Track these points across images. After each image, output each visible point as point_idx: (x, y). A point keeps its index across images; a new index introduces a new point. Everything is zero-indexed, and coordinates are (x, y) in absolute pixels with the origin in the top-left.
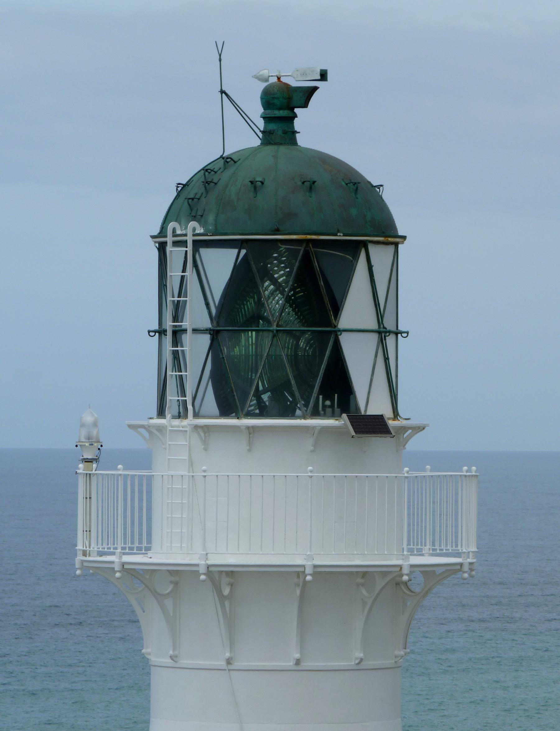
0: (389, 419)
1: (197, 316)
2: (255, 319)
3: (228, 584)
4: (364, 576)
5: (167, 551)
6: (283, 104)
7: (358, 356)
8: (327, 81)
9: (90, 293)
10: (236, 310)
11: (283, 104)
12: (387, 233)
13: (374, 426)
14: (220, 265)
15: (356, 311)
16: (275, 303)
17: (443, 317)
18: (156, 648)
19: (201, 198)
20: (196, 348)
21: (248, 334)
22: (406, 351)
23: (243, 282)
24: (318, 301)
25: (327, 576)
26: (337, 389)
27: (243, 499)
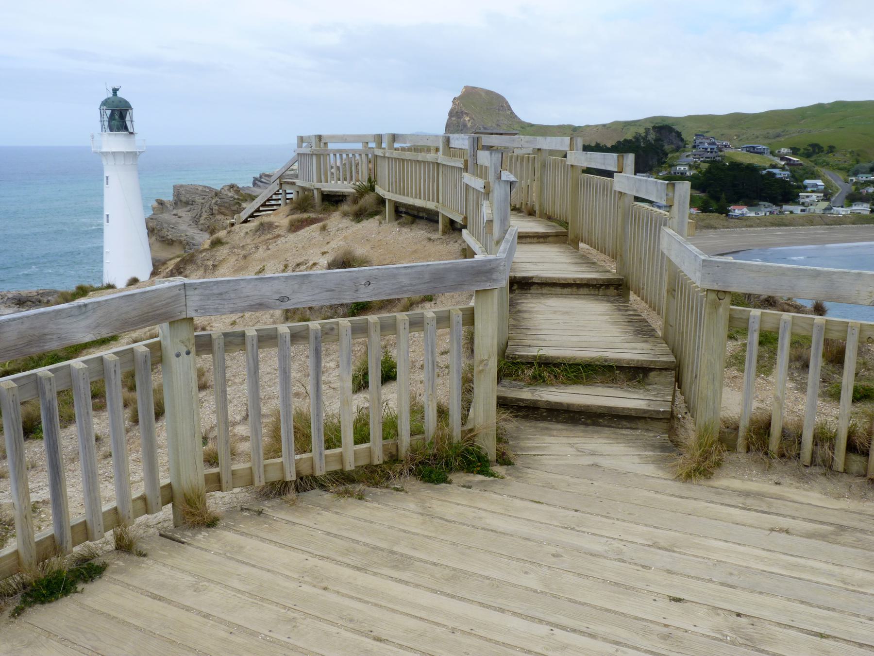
0: (746, 403)
1: (106, 119)
2: (114, 119)
3: (114, 154)
4: (132, 152)
5: (104, 150)
6: (115, 91)
7: (128, 124)
8: (174, 187)
9: (93, 117)
10: (111, 118)
11: (115, 91)
12: (130, 108)
13: (132, 133)
14: (109, 112)
15: (128, 118)
16: (117, 117)
17: (137, 118)
18: (104, 163)
19: (105, 103)
20: (106, 124)
21: (668, 395)
22: (134, 123)
23: (112, 115)
24: (122, 117)
25: (127, 152)
26: (126, 129)
27: (115, 142)
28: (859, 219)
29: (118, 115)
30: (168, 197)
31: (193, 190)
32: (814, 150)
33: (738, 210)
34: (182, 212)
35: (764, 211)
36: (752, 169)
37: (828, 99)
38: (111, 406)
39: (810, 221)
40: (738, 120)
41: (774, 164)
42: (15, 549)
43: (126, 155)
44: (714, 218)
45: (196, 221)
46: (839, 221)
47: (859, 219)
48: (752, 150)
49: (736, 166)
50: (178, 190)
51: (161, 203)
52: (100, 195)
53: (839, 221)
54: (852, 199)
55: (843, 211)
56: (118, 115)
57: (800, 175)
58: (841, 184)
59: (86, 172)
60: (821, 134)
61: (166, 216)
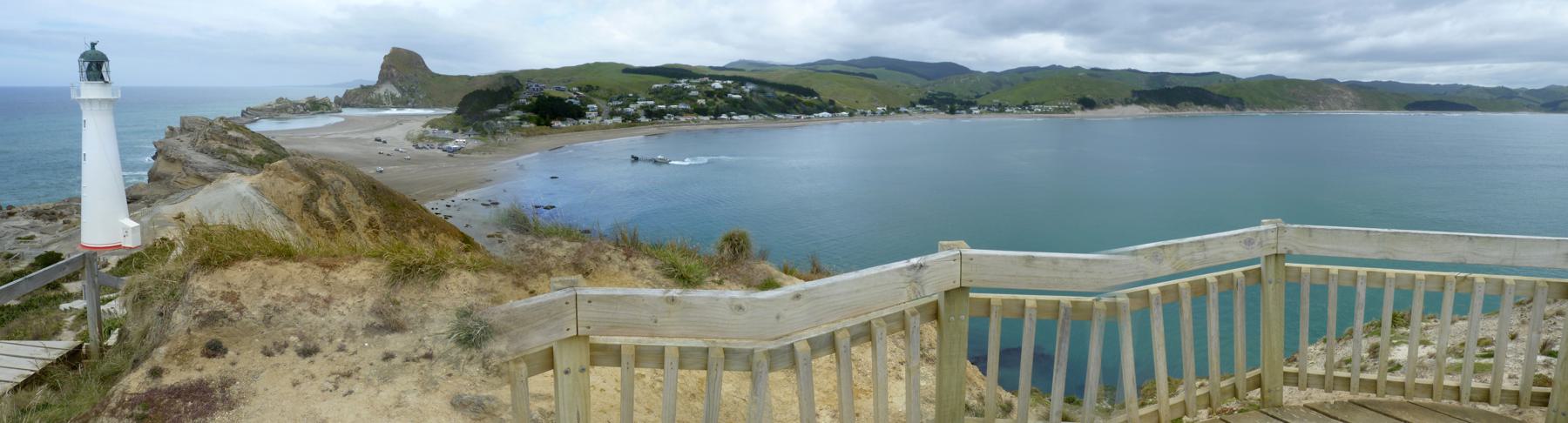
3: (90, 101)
6: (93, 45)
11: (93, 45)
17: (114, 69)
24: (99, 67)
27: (92, 91)
28: (617, 126)
29: (95, 66)
30: (177, 125)
31: (195, 120)
32: (588, 88)
33: (556, 124)
34: (184, 137)
35: (570, 123)
36: (560, 100)
37: (591, 61)
38: (1152, 118)
39: (594, 128)
40: (546, 72)
41: (571, 96)
42: (1517, 388)
43: (101, 101)
44: (544, 129)
45: (193, 144)
46: (608, 127)
47: (617, 126)
48: (558, 89)
49: (552, 98)
50: (183, 120)
51: (172, 129)
52: (79, 137)
53: (608, 127)
54: (612, 115)
55: (609, 122)
56: (95, 66)
57: (585, 101)
58: (603, 104)
59: (65, 109)
60: (589, 80)
61: (171, 140)
